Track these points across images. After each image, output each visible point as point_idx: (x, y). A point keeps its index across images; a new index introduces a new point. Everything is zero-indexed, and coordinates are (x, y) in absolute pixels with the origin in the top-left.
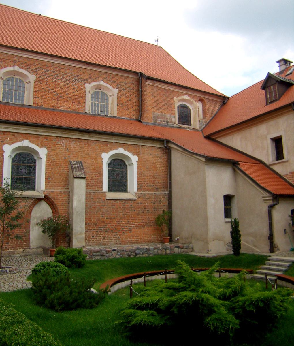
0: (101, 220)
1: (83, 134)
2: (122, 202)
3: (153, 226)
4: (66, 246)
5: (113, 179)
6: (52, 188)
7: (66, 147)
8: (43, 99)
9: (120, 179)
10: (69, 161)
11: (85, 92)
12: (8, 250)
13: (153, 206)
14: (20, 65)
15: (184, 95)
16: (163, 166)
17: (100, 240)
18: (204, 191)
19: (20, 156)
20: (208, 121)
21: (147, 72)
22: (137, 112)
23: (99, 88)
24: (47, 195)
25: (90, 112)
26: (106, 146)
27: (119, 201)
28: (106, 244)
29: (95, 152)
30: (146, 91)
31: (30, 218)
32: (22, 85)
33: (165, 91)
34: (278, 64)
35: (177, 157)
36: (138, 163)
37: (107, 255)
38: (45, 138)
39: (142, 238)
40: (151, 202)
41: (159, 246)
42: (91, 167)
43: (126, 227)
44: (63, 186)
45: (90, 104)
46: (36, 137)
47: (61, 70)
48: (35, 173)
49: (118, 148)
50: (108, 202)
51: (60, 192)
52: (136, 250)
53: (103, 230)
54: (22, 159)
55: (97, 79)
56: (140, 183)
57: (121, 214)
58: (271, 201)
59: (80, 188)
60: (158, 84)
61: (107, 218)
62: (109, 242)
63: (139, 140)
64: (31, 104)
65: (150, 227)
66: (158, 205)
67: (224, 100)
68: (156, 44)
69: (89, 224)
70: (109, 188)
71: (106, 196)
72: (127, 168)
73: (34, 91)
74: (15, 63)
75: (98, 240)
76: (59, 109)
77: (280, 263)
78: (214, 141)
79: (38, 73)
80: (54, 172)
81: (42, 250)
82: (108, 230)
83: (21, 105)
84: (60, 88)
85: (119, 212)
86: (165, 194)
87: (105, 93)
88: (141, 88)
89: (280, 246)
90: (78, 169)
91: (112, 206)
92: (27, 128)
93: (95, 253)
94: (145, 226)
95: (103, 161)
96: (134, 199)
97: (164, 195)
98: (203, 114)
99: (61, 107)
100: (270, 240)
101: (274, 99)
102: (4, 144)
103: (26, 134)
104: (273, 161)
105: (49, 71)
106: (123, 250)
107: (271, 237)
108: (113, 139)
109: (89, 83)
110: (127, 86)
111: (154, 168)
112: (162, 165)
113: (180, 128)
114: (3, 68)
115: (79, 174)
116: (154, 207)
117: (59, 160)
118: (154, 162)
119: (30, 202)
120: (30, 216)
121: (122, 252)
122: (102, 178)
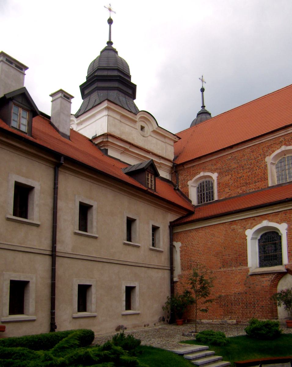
14: (287, 143)
24: (289, 268)
38: (284, 213)
46: (275, 215)
74: (282, 144)
92: (262, 209)
102: (246, 229)
114: (271, 154)
119: (272, 277)
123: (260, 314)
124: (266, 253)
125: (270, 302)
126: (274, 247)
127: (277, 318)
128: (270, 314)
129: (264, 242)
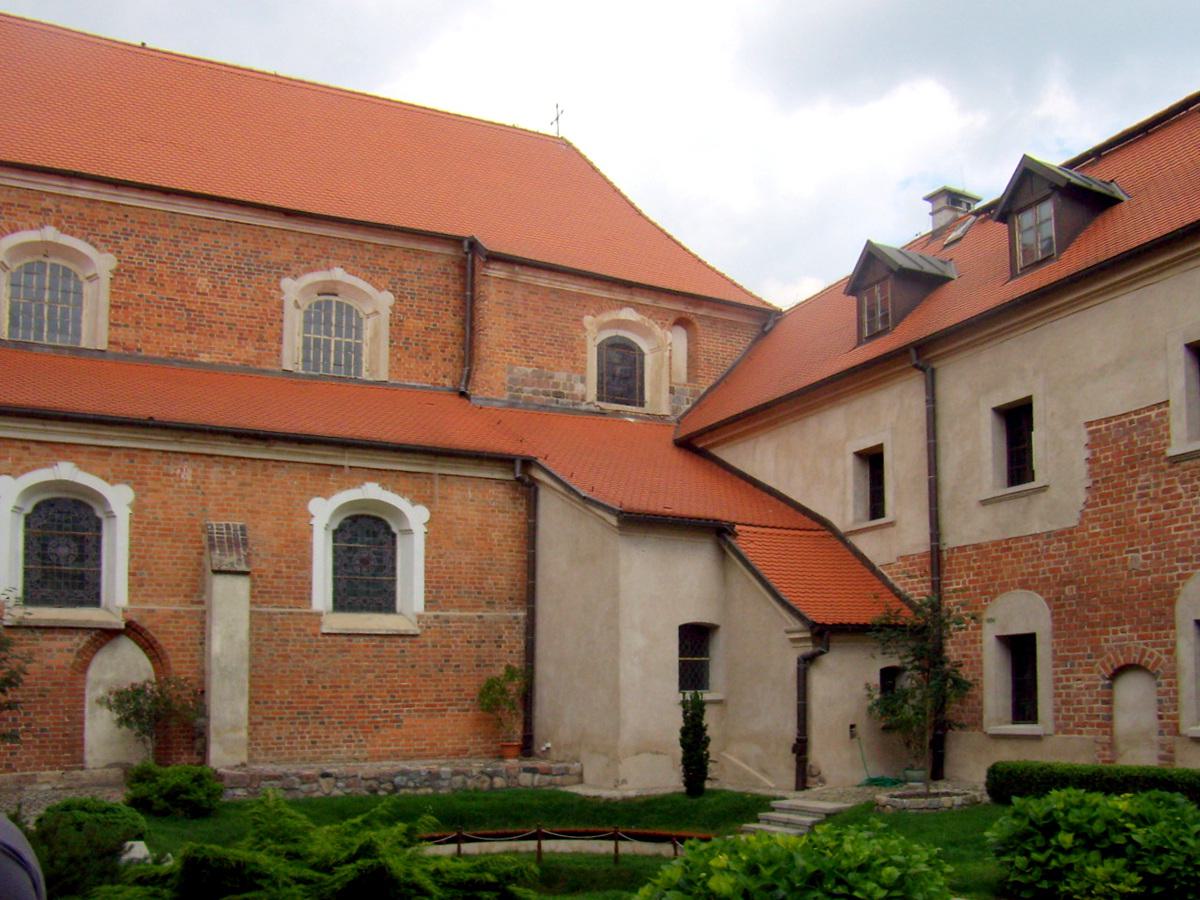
0: (304, 692)
1: (249, 444)
2: (372, 641)
3: (474, 710)
4: (195, 762)
5: (350, 574)
6: (149, 599)
7: (193, 482)
8: (141, 328)
9: (374, 575)
10: (203, 523)
11: (281, 305)
12: (15, 771)
13: (476, 654)
14: (63, 223)
15: (621, 308)
16: (510, 536)
17: (303, 748)
18: (614, 613)
19: (52, 510)
20: (702, 391)
21: (491, 243)
22: (458, 364)
23: (329, 290)
24: (135, 619)
25: (300, 368)
26: (323, 478)
27: (362, 639)
28: (319, 758)
29: (288, 496)
30: (486, 298)
31: (84, 684)
32: (72, 286)
33: (553, 296)
34: (928, 206)
35: (552, 510)
36: (428, 528)
37: (305, 787)
38: (127, 456)
39: (435, 744)
40: (469, 642)
41: (492, 765)
42: (275, 541)
43: (385, 712)
44: (186, 596)
45: (299, 342)
47: (200, 238)
48: (98, 558)
49: (363, 484)
50: (326, 641)
51: (176, 611)
52: (395, 776)
53: (311, 721)
54: (57, 516)
55: (323, 261)
56: (433, 587)
57: (370, 676)
58: (810, 644)
59: (231, 605)
60: (526, 276)
61: (324, 687)
62: (331, 752)
63: (433, 458)
64: (104, 346)
65: (461, 713)
66: (490, 651)
67: (765, 318)
68: (551, 131)
69: (266, 703)
70: (335, 600)
71: (320, 624)
72: (394, 543)
73: (112, 306)
74: (47, 218)
75: (296, 748)
76: (196, 359)
77: (793, 817)
78: (704, 455)
79: (122, 248)
80: (156, 556)
81: (122, 771)
82: (326, 720)
83: (70, 349)
84: (198, 293)
85: (365, 668)
86: (516, 618)
87: (349, 308)
88: (473, 290)
89: (825, 772)
90: (230, 547)
91: (341, 651)
93: (266, 780)
94: (445, 710)
95: (313, 522)
96: (411, 633)
97: (510, 622)
98: (688, 367)
99: (201, 355)
100: (799, 755)
101: (880, 327)
103: (64, 443)
104: (856, 521)
105: (158, 239)
106: (356, 776)
107: (801, 748)
108: (343, 458)
109: (296, 277)
110: (427, 284)
111: (482, 542)
112: (509, 534)
113: (603, 413)
114: (7, 234)
115: (230, 560)
116: (479, 656)
117: (170, 519)
118: (482, 525)
119: (80, 641)
120: (84, 679)
121: (351, 781)
122: (310, 573)
123: (33, 753)
124: (48, 562)
125: (69, 717)
126: (77, 549)
127: (80, 765)
128: (68, 755)
129: (44, 527)
